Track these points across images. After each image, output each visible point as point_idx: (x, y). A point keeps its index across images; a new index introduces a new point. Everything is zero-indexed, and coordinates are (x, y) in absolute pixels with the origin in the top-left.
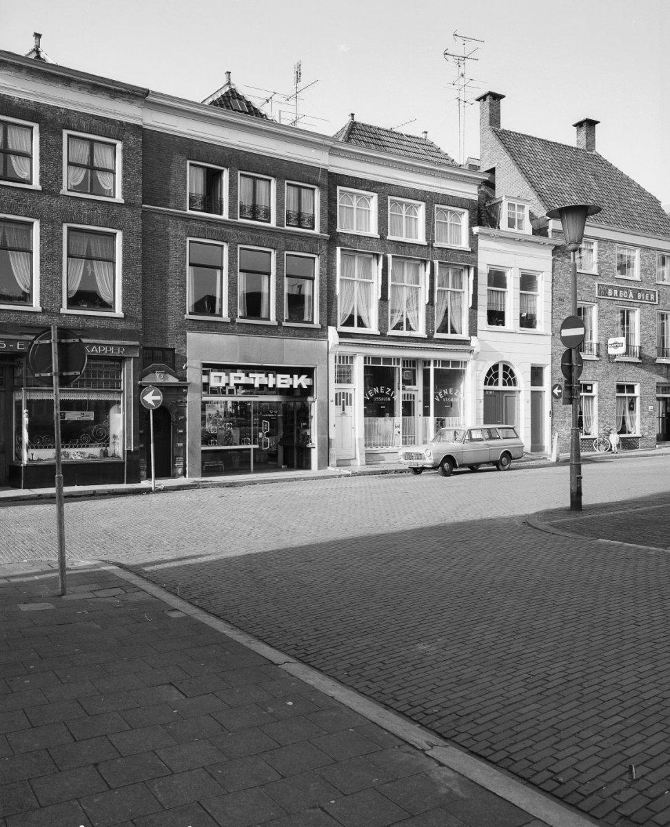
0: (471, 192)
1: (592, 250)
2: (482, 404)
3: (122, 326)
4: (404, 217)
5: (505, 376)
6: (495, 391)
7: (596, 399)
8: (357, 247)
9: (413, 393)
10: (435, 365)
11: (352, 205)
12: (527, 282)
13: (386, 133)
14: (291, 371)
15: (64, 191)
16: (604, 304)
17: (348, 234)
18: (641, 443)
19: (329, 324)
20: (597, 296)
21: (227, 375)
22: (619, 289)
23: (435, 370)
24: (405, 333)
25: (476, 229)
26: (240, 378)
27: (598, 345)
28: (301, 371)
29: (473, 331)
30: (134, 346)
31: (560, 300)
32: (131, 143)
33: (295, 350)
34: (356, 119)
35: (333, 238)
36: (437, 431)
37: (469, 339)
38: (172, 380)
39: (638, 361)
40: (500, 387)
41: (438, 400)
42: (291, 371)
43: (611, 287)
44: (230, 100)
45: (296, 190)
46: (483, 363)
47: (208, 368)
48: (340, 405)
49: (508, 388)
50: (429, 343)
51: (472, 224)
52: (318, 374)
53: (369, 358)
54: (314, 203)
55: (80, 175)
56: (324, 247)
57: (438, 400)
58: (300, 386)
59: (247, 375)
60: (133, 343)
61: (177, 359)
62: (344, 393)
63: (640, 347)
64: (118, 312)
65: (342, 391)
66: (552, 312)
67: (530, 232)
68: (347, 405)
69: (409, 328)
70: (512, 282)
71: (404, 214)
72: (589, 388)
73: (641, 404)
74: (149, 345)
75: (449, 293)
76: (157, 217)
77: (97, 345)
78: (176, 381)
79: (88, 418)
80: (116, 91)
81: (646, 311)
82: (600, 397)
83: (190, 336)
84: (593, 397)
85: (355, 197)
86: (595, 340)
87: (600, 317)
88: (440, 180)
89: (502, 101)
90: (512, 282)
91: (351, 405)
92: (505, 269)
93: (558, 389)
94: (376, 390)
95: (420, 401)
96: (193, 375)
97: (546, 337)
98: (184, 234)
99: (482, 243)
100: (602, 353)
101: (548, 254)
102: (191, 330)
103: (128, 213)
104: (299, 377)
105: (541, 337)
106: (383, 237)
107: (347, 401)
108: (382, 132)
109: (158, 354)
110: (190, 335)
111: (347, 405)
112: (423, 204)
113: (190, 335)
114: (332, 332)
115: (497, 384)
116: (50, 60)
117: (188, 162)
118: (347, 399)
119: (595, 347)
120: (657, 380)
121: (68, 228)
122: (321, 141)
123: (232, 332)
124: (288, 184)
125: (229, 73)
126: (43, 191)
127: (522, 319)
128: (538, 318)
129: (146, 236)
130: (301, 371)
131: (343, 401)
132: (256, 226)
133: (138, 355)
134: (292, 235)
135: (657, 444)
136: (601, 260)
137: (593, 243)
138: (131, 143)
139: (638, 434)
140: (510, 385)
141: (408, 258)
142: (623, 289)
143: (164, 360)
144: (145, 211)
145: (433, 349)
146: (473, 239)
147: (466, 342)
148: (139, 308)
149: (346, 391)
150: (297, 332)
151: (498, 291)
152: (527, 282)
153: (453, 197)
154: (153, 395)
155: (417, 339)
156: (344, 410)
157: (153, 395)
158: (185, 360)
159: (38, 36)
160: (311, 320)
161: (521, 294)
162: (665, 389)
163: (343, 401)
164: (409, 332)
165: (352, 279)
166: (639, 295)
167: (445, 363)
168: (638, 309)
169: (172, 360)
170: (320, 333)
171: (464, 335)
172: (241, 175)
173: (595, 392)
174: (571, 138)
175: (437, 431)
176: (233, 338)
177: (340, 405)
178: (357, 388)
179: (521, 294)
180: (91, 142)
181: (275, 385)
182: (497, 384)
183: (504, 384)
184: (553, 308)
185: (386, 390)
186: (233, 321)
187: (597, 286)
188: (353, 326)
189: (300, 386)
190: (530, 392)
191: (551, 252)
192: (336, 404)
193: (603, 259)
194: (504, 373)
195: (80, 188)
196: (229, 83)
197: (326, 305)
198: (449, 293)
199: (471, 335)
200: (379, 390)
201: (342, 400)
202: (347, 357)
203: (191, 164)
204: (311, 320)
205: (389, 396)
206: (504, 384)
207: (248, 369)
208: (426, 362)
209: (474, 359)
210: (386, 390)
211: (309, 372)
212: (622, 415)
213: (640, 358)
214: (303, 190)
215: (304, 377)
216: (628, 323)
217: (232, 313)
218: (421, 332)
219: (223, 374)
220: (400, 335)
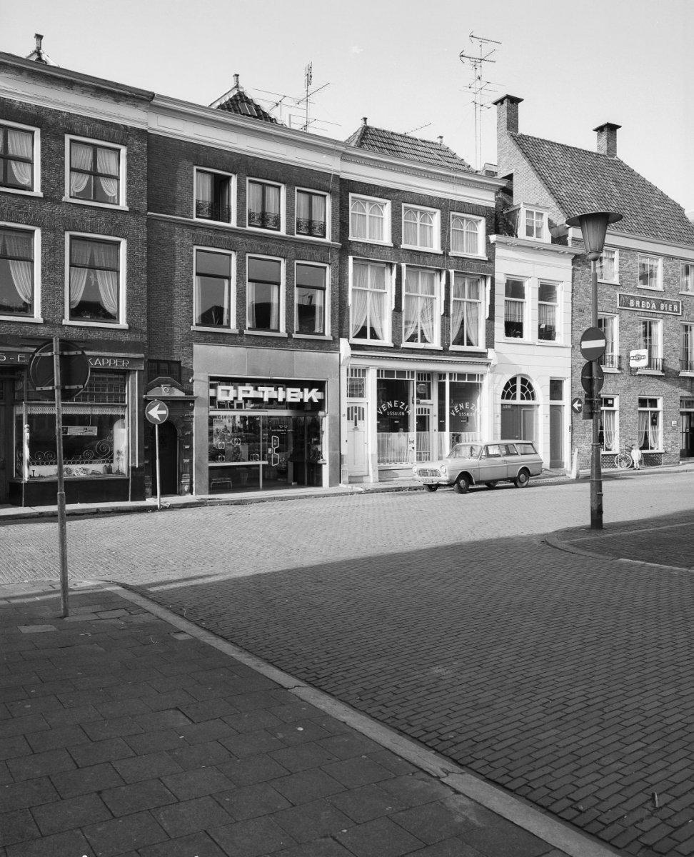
0: (488, 199)
1: (613, 259)
2: (499, 419)
3: (126, 338)
4: (418, 225)
5: (523, 389)
6: (513, 405)
7: (617, 414)
8: (370, 256)
9: (427, 407)
10: (450, 378)
12: (546, 292)
14: (301, 385)
15: (66, 198)
16: (626, 315)
17: (360, 243)
18: (664, 459)
19: (341, 335)
20: (618, 306)
21: (235, 388)
22: (642, 299)
23: (451, 383)
24: (419, 345)
25: (493, 238)
26: (248, 392)
27: (620, 357)
28: (311, 385)
29: (490, 343)
30: (139, 359)
31: (580, 311)
32: (136, 149)
33: (305, 363)
34: (369, 124)
35: (345, 247)
37: (485, 351)
38: (178, 393)
39: (661, 374)
40: (518, 401)
41: (454, 414)
42: (301, 385)
43: (633, 297)
44: (238, 104)
45: (307, 196)
46: (500, 376)
47: (215, 381)
48: (352, 419)
49: (526, 402)
50: (444, 355)
51: (489, 232)
52: (329, 388)
53: (382, 371)
54: (326, 210)
55: (83, 181)
56: (336, 256)
57: (454, 414)
58: (311, 400)
59: (256, 389)
60: (137, 356)
61: (184, 372)
62: (356, 407)
63: (663, 360)
64: (123, 323)
65: (354, 405)
66: (572, 323)
68: (359, 419)
69: (424, 340)
70: (531, 292)
71: (418, 221)
72: (610, 402)
73: (664, 418)
74: (154, 357)
75: (465, 303)
76: (163, 225)
77: (101, 357)
79: (91, 434)
80: (120, 94)
81: (669, 322)
82: (621, 411)
83: (197, 348)
84: (614, 411)
85: (367, 204)
86: (616, 353)
87: (622, 328)
88: (456, 186)
89: (520, 104)
90: (531, 292)
91: (363, 419)
92: (523, 278)
93: (578, 403)
94: (390, 404)
96: (200, 389)
97: (566, 349)
99: (499, 252)
100: (624, 366)
101: (567, 263)
102: (198, 342)
103: (132, 221)
104: (309, 391)
105: (560, 349)
106: (396, 246)
107: (359, 416)
109: (164, 366)
110: (196, 347)
111: (359, 419)
112: (438, 212)
113: (196, 347)
115: (514, 398)
118: (359, 414)
119: (616, 359)
120: (680, 394)
122: (332, 146)
123: (241, 344)
125: (237, 75)
126: (45, 198)
127: (540, 330)
128: (557, 330)
129: (151, 245)
130: (311, 385)
131: (356, 416)
132: (265, 234)
133: (143, 368)
134: (303, 244)
135: (681, 460)
136: (623, 269)
137: (614, 252)
138: (136, 149)
139: (661, 450)
140: (529, 399)
141: (423, 268)
142: (645, 299)
144: (150, 219)
145: (449, 362)
146: (490, 247)
147: (483, 355)
148: (144, 319)
149: (358, 405)
150: (307, 344)
151: (516, 302)
152: (546, 292)
153: (469, 204)
155: (432, 352)
156: (356, 425)
158: (191, 373)
159: (39, 37)
161: (539, 305)
162: (689, 403)
163: (356, 416)
164: (423, 344)
165: (364, 289)
166: (662, 306)
167: (461, 376)
168: (661, 320)
169: (178, 373)
170: (331, 345)
171: (481, 347)
173: (616, 407)
174: (591, 143)
176: (241, 350)
177: (352, 419)
178: (370, 402)
179: (539, 305)
181: (284, 399)
182: (514, 398)
183: (522, 398)
184: (572, 320)
185: (399, 404)
187: (618, 297)
188: (366, 338)
189: (311, 400)
190: (549, 406)
191: (570, 261)
192: (348, 419)
193: (625, 268)
194: (522, 387)
195: (82, 195)
196: (237, 86)
197: (337, 316)
199: (487, 347)
200: (393, 404)
201: (354, 414)
202: (359, 370)
205: (403, 411)
206: (522, 398)
207: (256, 383)
208: (442, 375)
210: (399, 404)
211: (320, 385)
212: (644, 430)
213: (663, 371)
214: (313, 197)
215: (314, 390)
216: (650, 335)
217: (241, 324)
218: (436, 344)
219: (231, 388)
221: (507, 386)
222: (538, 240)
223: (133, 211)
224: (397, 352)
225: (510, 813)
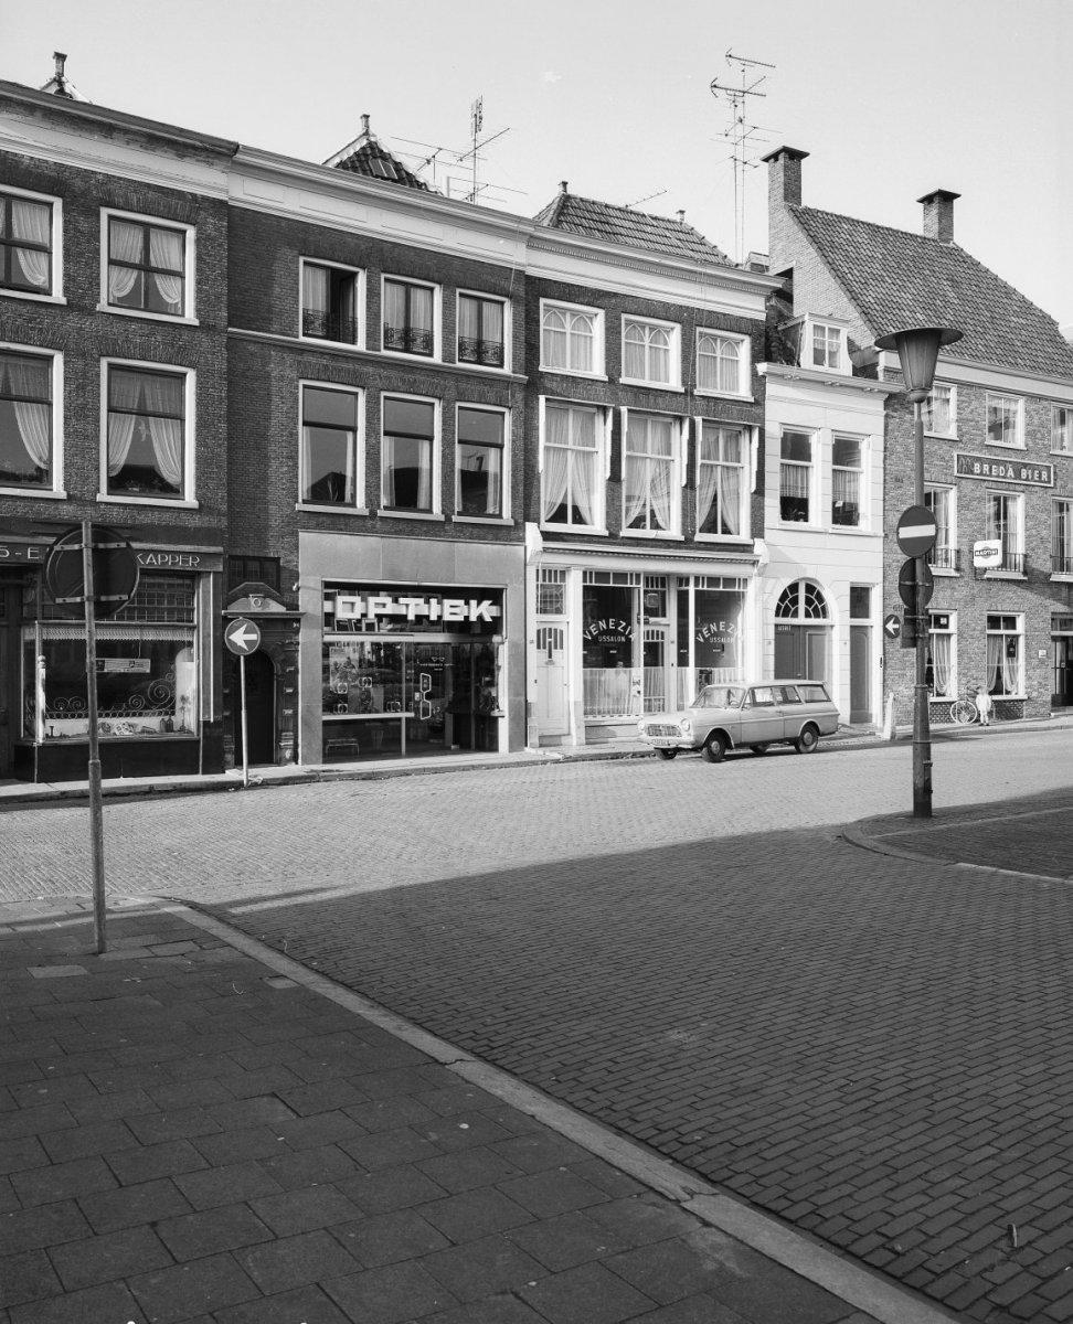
0: (754, 308)
1: (948, 400)
2: (772, 647)
3: (195, 522)
4: (647, 347)
5: (809, 602)
6: (793, 626)
7: (954, 639)
8: (572, 395)
9: (661, 629)
10: (696, 584)
11: (564, 327)
12: (845, 451)
13: (618, 214)
14: (466, 594)
15: (102, 306)
16: (968, 486)
17: (557, 375)
18: (1026, 709)
19: (527, 518)
20: (956, 473)
21: (364, 600)
22: (992, 462)
23: (697, 592)
24: (648, 533)
25: (762, 367)
26: (384, 605)
27: (958, 552)
28: (481, 594)
29: (758, 530)
30: (215, 554)
31: (897, 480)
32: (210, 229)
33: (472, 561)
34: (570, 191)
35: (534, 382)
36: (700, 690)
37: (751, 542)
38: (275, 608)
39: (1022, 578)
40: (801, 620)
41: (702, 640)
42: (466, 594)
43: (978, 459)
44: (368, 161)
46: (774, 580)
47: (333, 589)
48: (544, 648)
49: (813, 621)
50: (686, 548)
51: (756, 358)
52: (509, 599)
53: (591, 573)
54: (503, 324)
55: (129, 280)
56: (520, 396)
57: (702, 640)
58: (480, 617)
59: (396, 601)
60: (213, 549)
61: (284, 575)
62: (550, 629)
63: (1026, 556)
64: (190, 499)
65: (548, 626)
66: (884, 500)
67: (849, 372)
68: (556, 648)
69: (656, 526)
70: (821, 451)
71: (647, 342)
72: (943, 621)
73: (1027, 646)
74: (238, 552)
75: (719, 469)
76: (252, 348)
77: (155, 552)
78: (282, 609)
79: (141, 670)
80: (186, 146)
82: (960, 635)
83: (305, 537)
84: (949, 636)
85: (568, 315)
87: (961, 507)
88: (705, 288)
89: (803, 161)
90: (821, 451)
91: (562, 648)
92: (808, 430)
93: (894, 623)
94: (602, 624)
95: (672, 642)
96: (310, 600)
97: (875, 539)
98: (294, 375)
99: (772, 389)
100: (964, 565)
101: (877, 407)
102: (306, 528)
103: (205, 341)
104: (479, 604)
105: (867, 539)
106: (613, 380)
107: (556, 642)
108: (611, 212)
109: (254, 566)
110: (304, 536)
111: (556, 648)
112: (678, 327)
113: (304, 536)
114: (532, 532)
115: (795, 614)
116: (80, 97)
117: (302, 259)
118: (556, 639)
119: (952, 555)
120: (1052, 609)
121: (109, 364)
122: (513, 225)
123: (372, 531)
124: (461, 295)
125: (367, 117)
126: (70, 306)
127: (835, 510)
128: (862, 510)
129: (233, 378)
130: (481, 594)
131: (550, 643)
132: (410, 361)
133: (221, 569)
134: (468, 376)
135: (1052, 711)
136: (963, 416)
137: (949, 389)
138: (210, 229)
139: (1022, 695)
140: (817, 616)
141: (653, 414)
142: (997, 462)
143: (262, 576)
144: (232, 338)
145: (694, 559)
146: (758, 382)
147: (746, 548)
148: (222, 493)
149: (553, 626)
150: (475, 531)
151: (797, 467)
152: (845, 451)
153: (725, 315)
154: (245, 633)
155: (668, 543)
156: (550, 656)
157: (245, 633)
158: (296, 576)
159: (61, 57)
160: (497, 513)
161: (834, 471)
162: (1065, 623)
163: (550, 643)
164: (654, 531)
165: (563, 446)
166: (1024, 473)
167: (713, 581)
168: (1023, 495)
169: (275, 576)
170: (512, 534)
171: (744, 536)
172: (387, 280)
173: (953, 628)
174: (914, 221)
175: (700, 690)
176: (372, 541)
177: (544, 648)
178: (572, 621)
179: (834, 471)
180: (147, 227)
181: (440, 617)
182: (795, 614)
183: (808, 615)
184: (885, 494)
185: (617, 624)
187: (956, 458)
188: (566, 522)
189: (480, 617)
190: (848, 628)
191: (882, 403)
192: (539, 647)
193: (966, 414)
194: (807, 597)
195: (127, 301)
196: (367, 134)
197: (521, 488)
198: (719, 469)
199: (754, 536)
200: (608, 625)
201: (548, 640)
202: (556, 571)
203: (305, 263)
204: (497, 513)
205: (623, 634)
206: (808, 615)
207: (397, 591)
208: (683, 580)
210: (617, 624)
211: (495, 596)
212: (996, 665)
213: (1025, 573)
214: (485, 304)
215: (486, 603)
216: (1005, 518)
217: (372, 500)
218: (674, 532)
219: (357, 599)
220: (640, 536)
221: (783, 597)
223: (205, 327)
224: (614, 544)
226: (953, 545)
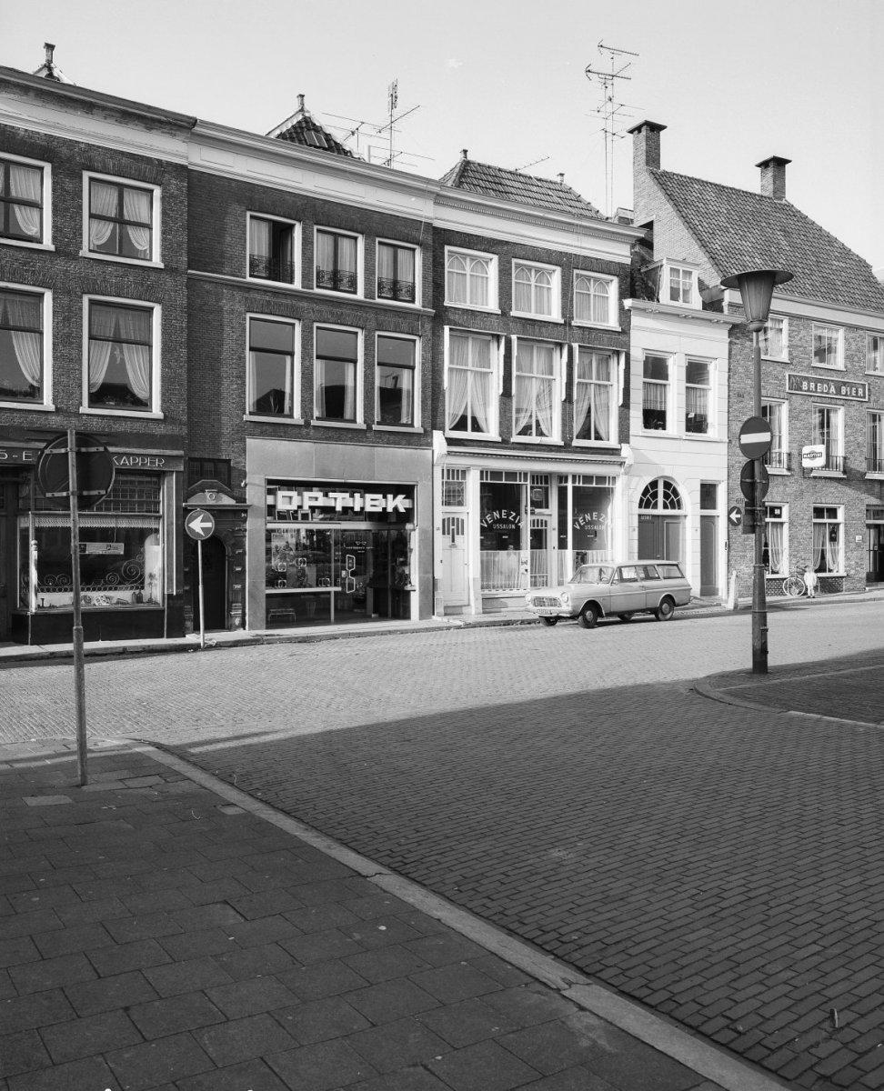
0: (621, 254)
1: (781, 330)
2: (636, 533)
3: (161, 430)
4: (533, 286)
5: (666, 496)
6: (653, 516)
7: (786, 527)
8: (471, 325)
9: (544, 518)
10: (574, 482)
12: (696, 372)
14: (384, 490)
15: (84, 252)
16: (797, 401)
17: (459, 309)
18: (845, 585)
19: (434, 427)
20: (787, 390)
21: (300, 494)
22: (817, 381)
23: (574, 488)
24: (534, 439)
25: (628, 303)
26: (316, 499)
27: (789, 455)
28: (397, 490)
29: (624, 437)
30: (177, 456)
31: (739, 395)
32: (173, 189)
33: (389, 462)
34: (470, 157)
35: (440, 315)
36: (577, 568)
37: (618, 447)
38: (227, 501)
39: (842, 476)
40: (660, 511)
41: (578, 528)
42: (384, 490)
43: (806, 378)
44: (303, 132)
45: (391, 250)
46: (637, 478)
47: (274, 485)
48: (449, 534)
49: (670, 512)
50: (565, 452)
52: (419, 493)
53: (487, 472)
54: (415, 267)
55: (106, 230)
56: (428, 326)
57: (578, 528)
58: (396, 509)
59: (326, 495)
60: (175, 453)
62: (453, 519)
63: (845, 458)
64: (156, 411)
65: (451, 516)
66: (728, 412)
68: (458, 534)
69: (540, 433)
70: (676, 371)
71: (533, 282)
72: (777, 512)
73: (846, 532)
74: (196, 455)
75: (593, 386)
76: (207, 287)
77: (128, 455)
79: (116, 552)
80: (153, 120)
82: (791, 523)
83: (251, 443)
84: (782, 524)
87: (792, 418)
88: (581, 237)
90: (676, 371)
91: (463, 534)
92: (666, 354)
93: (737, 513)
94: (496, 515)
95: (554, 529)
96: (255, 495)
97: (721, 444)
99: (636, 320)
100: (795, 466)
101: (722, 335)
102: (252, 435)
103: (169, 281)
104: (394, 498)
105: (714, 445)
106: (505, 313)
107: (458, 529)
109: (209, 466)
110: (250, 442)
111: (458, 534)
112: (558, 270)
113: (250, 442)
115: (655, 506)
118: (458, 527)
119: (785, 458)
120: (867, 502)
122: (423, 186)
123: (306, 438)
125: (302, 96)
126: (57, 252)
127: (688, 420)
128: (710, 420)
129: (192, 311)
130: (397, 490)
131: (453, 530)
132: (338, 298)
133: (182, 469)
134: (385, 310)
135: (867, 586)
136: (794, 343)
137: (782, 321)
138: (173, 189)
139: (842, 573)
140: (673, 507)
141: (538, 341)
142: (822, 381)
144: (191, 279)
145: (572, 461)
146: (625, 315)
147: (615, 452)
148: (183, 406)
149: (456, 516)
150: (392, 438)
151: (657, 384)
152: (696, 372)
153: (597, 259)
154: (202, 521)
155: (550, 448)
156: (453, 541)
157: (202, 521)
158: (244, 475)
159: (50, 47)
161: (687, 388)
162: (877, 513)
163: (453, 530)
164: (539, 438)
165: (464, 368)
166: (844, 390)
167: (587, 478)
168: (842, 408)
169: (226, 475)
170: (422, 440)
171: (613, 442)
173: (785, 518)
175: (577, 568)
176: (307, 446)
177: (449, 534)
178: (471, 511)
179: (687, 388)
181: (362, 509)
182: (655, 506)
183: (665, 507)
184: (729, 407)
185: (509, 515)
186: (307, 424)
187: (787, 378)
188: (466, 430)
189: (396, 509)
190: (699, 517)
191: (727, 332)
192: (444, 533)
193: (796, 341)
194: (665, 492)
195: (105, 248)
196: (302, 110)
197: (429, 402)
199: (621, 441)
200: (501, 515)
201: (451, 527)
202: (458, 471)
205: (513, 523)
206: (665, 507)
207: (327, 487)
208: (563, 478)
209: (626, 474)
210: (509, 515)
211: (408, 491)
212: (820, 548)
213: (844, 472)
214: (399, 251)
215: (400, 497)
216: (828, 427)
217: (307, 412)
218: (555, 438)
219: (294, 494)
222: (685, 305)
224: (506, 448)
225: (650, 1035)
226: (785, 449)
